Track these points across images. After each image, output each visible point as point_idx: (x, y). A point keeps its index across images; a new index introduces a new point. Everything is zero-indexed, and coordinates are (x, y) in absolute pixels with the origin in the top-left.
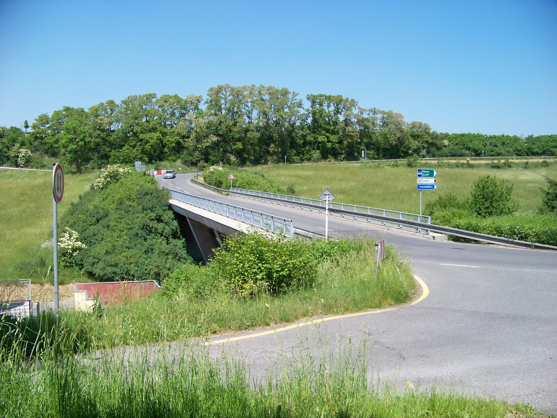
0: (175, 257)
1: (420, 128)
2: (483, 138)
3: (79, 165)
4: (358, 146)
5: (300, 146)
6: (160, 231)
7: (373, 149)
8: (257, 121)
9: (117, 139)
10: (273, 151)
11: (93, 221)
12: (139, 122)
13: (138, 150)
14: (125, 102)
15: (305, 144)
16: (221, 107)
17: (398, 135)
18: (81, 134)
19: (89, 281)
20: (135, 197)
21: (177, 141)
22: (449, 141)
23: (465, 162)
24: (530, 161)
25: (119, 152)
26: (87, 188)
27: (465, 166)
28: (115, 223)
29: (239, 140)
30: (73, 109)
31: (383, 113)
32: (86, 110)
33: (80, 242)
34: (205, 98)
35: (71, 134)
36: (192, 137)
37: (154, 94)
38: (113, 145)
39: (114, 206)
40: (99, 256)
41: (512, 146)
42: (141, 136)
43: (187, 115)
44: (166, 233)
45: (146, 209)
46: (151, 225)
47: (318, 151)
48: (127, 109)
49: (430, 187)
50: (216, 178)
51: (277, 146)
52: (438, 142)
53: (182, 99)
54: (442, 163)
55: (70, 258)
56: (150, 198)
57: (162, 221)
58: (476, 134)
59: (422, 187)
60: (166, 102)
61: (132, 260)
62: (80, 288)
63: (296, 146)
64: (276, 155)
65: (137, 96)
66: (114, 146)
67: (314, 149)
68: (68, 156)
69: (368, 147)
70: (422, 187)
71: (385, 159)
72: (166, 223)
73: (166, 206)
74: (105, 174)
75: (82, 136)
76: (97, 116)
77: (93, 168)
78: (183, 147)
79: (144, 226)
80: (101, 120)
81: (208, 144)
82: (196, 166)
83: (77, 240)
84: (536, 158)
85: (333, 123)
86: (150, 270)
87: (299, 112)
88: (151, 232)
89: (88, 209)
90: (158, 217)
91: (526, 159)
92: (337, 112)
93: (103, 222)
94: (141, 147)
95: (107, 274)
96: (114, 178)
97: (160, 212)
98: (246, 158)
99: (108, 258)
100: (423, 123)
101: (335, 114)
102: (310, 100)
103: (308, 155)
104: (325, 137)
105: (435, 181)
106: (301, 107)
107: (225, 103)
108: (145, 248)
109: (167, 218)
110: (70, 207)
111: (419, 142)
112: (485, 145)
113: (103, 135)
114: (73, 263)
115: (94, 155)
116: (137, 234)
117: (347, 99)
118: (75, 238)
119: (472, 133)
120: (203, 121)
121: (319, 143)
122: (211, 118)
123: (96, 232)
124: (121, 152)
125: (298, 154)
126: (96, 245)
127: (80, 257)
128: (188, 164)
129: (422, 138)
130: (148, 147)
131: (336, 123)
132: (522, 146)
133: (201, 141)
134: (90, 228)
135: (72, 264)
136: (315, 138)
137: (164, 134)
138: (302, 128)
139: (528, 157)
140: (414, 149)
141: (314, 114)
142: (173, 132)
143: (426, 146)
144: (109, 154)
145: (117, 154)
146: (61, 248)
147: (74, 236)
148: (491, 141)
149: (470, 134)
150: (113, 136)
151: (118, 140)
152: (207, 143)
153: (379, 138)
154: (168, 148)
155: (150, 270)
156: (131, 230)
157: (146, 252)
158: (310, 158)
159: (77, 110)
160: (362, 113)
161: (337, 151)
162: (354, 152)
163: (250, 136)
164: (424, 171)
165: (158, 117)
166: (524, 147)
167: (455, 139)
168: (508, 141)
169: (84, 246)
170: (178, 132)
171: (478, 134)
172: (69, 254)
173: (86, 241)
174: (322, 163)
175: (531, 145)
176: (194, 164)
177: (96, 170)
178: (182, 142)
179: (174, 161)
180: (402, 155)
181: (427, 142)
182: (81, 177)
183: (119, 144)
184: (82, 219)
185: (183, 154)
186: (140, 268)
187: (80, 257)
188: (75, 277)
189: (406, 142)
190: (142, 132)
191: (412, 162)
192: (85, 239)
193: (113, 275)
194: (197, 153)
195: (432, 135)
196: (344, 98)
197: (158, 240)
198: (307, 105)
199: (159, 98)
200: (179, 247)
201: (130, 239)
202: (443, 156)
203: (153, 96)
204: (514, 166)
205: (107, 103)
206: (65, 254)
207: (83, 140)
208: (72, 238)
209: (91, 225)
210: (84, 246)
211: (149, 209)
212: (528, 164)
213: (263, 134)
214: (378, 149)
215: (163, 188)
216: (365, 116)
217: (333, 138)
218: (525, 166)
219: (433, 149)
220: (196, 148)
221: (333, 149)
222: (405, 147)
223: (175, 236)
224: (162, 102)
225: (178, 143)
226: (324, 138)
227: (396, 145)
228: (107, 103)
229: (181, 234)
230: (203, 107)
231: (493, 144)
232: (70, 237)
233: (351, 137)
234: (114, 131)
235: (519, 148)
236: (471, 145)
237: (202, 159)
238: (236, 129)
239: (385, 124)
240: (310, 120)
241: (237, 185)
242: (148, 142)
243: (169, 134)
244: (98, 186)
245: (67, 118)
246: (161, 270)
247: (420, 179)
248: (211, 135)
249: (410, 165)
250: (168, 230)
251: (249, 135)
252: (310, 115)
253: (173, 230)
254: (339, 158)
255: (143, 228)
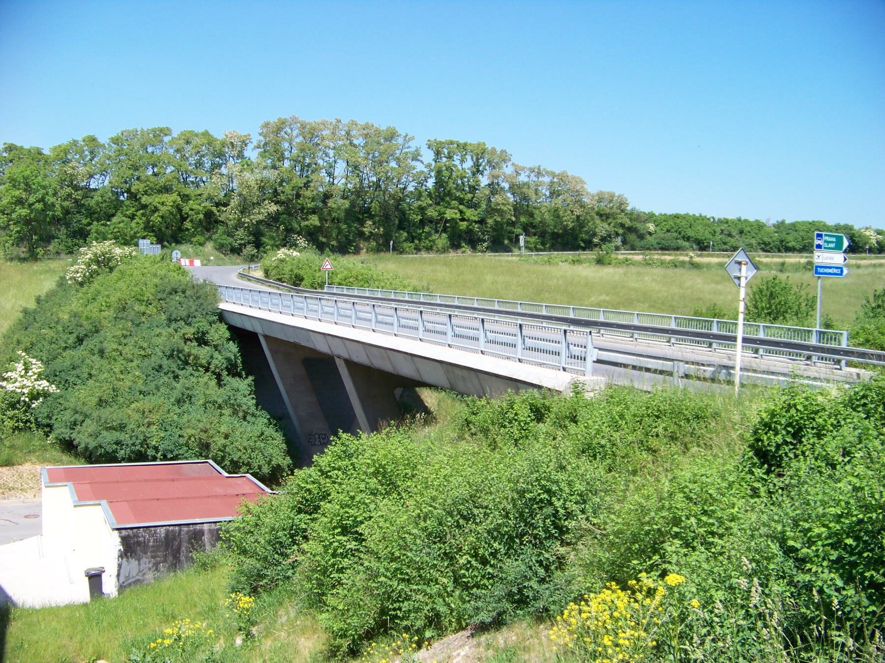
0: (235, 413)
1: (611, 201)
2: (709, 222)
3: (32, 246)
4: (509, 228)
5: (414, 225)
6: (204, 362)
7: (535, 234)
8: (344, 181)
9: (102, 203)
10: (371, 233)
11: (70, 341)
12: (141, 174)
13: (138, 223)
14: (116, 141)
15: (422, 223)
16: (283, 154)
17: (578, 212)
18: (38, 190)
19: (65, 458)
20: (151, 297)
21: (208, 210)
22: (656, 226)
23: (687, 259)
24: (788, 260)
25: (105, 225)
26: (48, 284)
27: (687, 266)
28: (115, 346)
29: (314, 211)
30: (22, 148)
31: (553, 175)
32: (46, 152)
33: (45, 381)
34: (256, 139)
35: (19, 189)
36: (232, 204)
37: (168, 129)
38: (94, 213)
39: (110, 313)
40: (85, 409)
41: (755, 236)
42: (145, 200)
43: (224, 166)
44: (216, 367)
45: (176, 320)
46: (186, 349)
47: (444, 235)
48: (120, 152)
49: (835, 271)
50: (291, 271)
51: (377, 225)
52: (639, 226)
53: (216, 140)
54: (650, 259)
55: (26, 411)
56: (182, 299)
57: (206, 343)
58: (697, 215)
59: (821, 270)
60: (188, 143)
61: (154, 417)
62: (55, 479)
63: (409, 226)
64: (374, 239)
65: (137, 131)
66: (96, 215)
67: (437, 232)
68: (15, 229)
69: (527, 229)
70: (821, 270)
71: (555, 250)
72: (216, 347)
73: (214, 314)
74: (88, 256)
75: (39, 195)
76: (65, 162)
77: (58, 253)
78: (217, 222)
79: (173, 351)
80: (73, 168)
81: (261, 217)
82: (239, 254)
83: (40, 377)
84: (795, 257)
85: (470, 188)
86: (190, 438)
87: (414, 169)
88: (186, 363)
89: (59, 318)
90: (200, 335)
91: (781, 257)
92: (477, 170)
93: (88, 343)
94: (144, 219)
95: (104, 445)
96: (105, 266)
97: (204, 325)
98: (323, 243)
99: (105, 413)
100: (616, 195)
101: (474, 174)
102: (432, 149)
103: (427, 241)
104: (457, 211)
105: (845, 259)
106: (419, 160)
107: (290, 149)
108: (176, 394)
109: (216, 337)
110: (21, 315)
111: (609, 224)
112: (714, 233)
113: (77, 195)
114: (31, 423)
115: (59, 231)
116: (160, 366)
117: (494, 149)
118: (35, 374)
119: (691, 214)
120: (251, 178)
121: (447, 221)
122: (266, 173)
123: (78, 362)
124: (109, 226)
125: (411, 239)
126: (76, 387)
127: (45, 411)
128: (226, 251)
129: (614, 219)
130: (156, 218)
131: (473, 189)
132: (771, 237)
133: (249, 212)
134: (64, 354)
135: (28, 424)
136: (441, 214)
137: (186, 198)
138: (419, 196)
139: (780, 254)
140: (602, 236)
141: (439, 172)
142: (200, 195)
143: (621, 231)
144: (88, 228)
145: (102, 229)
146: (6, 393)
147: (34, 370)
148: (723, 228)
149: (687, 214)
150: (96, 198)
151: (104, 205)
152: (259, 215)
153: (547, 216)
154: (192, 221)
155: (190, 438)
156: (146, 359)
157: (179, 402)
158: (431, 246)
159: (30, 151)
160: (518, 174)
161: (477, 235)
162: (504, 239)
163: (334, 206)
164: (827, 238)
165: (173, 168)
166: (775, 239)
167: (665, 223)
168: (748, 229)
169: (53, 389)
170: (209, 194)
171: (701, 216)
172: (22, 404)
173: (57, 379)
174: (452, 255)
175: (784, 236)
176: (236, 251)
177: (63, 256)
178: (216, 211)
179: (202, 244)
180: (582, 244)
181: (622, 225)
182: (36, 267)
183: (105, 213)
184: (48, 337)
185: (216, 232)
186: (169, 433)
187: (45, 410)
188: (34, 451)
189: (590, 224)
190: (146, 193)
191: (603, 257)
192: (56, 376)
193: (115, 447)
194: (241, 233)
195: (630, 214)
196: (489, 146)
197: (200, 379)
198: (428, 156)
199: (176, 136)
200: (242, 392)
201: (147, 376)
202: (649, 249)
203: (165, 131)
204: (764, 268)
205: (84, 141)
206: (15, 404)
207: (42, 200)
208: (30, 373)
209: (66, 348)
210: (53, 389)
211: (181, 319)
212: (785, 266)
213: (353, 205)
214: (542, 235)
215: (205, 281)
216: (523, 178)
217: (470, 213)
218: (780, 268)
219: (632, 237)
220: (239, 224)
221: (469, 232)
222: (587, 233)
223: (232, 371)
224: (181, 142)
225: (209, 214)
226: (456, 214)
227: (573, 229)
228: (84, 141)
229: (243, 369)
230: (252, 154)
231: (726, 232)
232: (27, 370)
233: (501, 212)
234: (95, 190)
235: (766, 239)
236: (690, 233)
237: (250, 243)
238: (308, 193)
239: (554, 194)
240: (430, 183)
241: (337, 280)
242: (156, 210)
243: (193, 198)
244: (75, 278)
245: (10, 164)
246: (212, 437)
247: (819, 254)
248: (267, 202)
249: (600, 262)
250: (219, 361)
251: (331, 203)
252: (433, 174)
253: (228, 359)
254: (479, 247)
255: (171, 356)
